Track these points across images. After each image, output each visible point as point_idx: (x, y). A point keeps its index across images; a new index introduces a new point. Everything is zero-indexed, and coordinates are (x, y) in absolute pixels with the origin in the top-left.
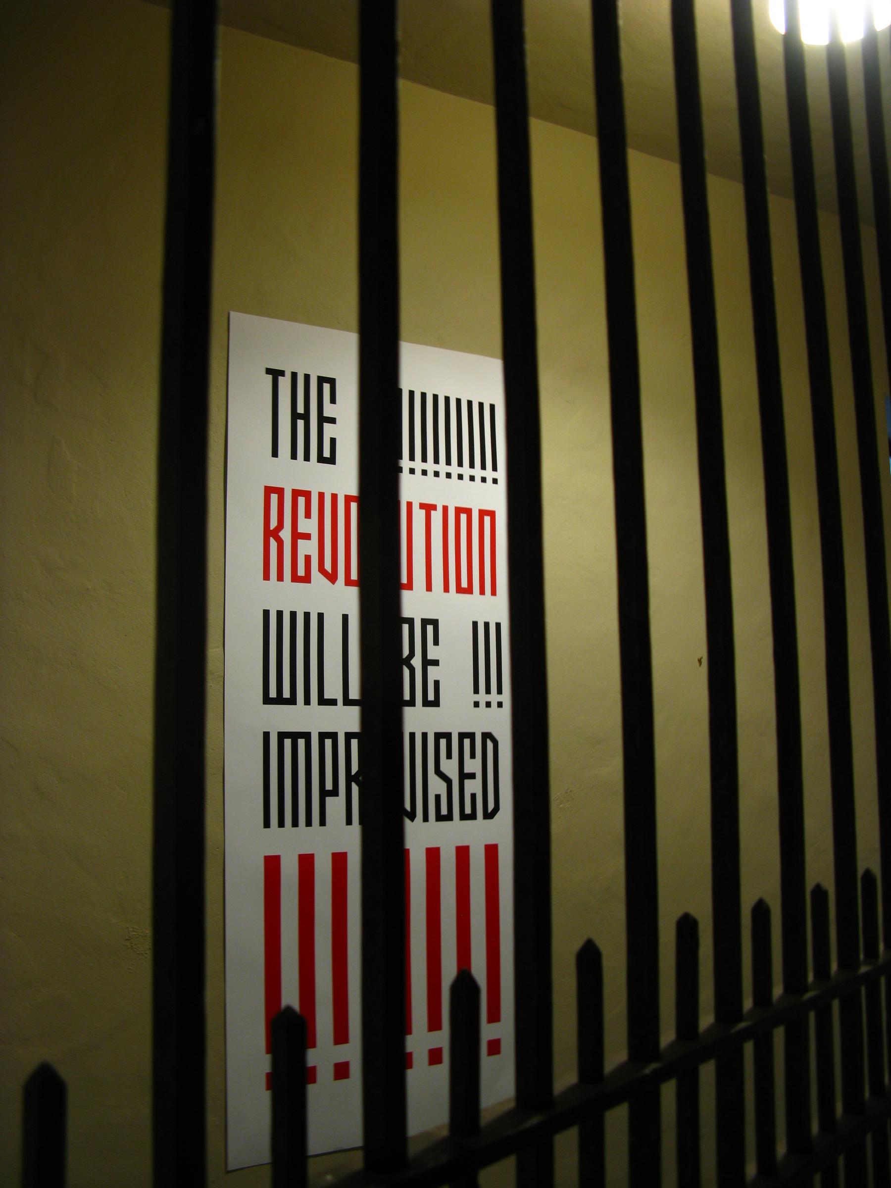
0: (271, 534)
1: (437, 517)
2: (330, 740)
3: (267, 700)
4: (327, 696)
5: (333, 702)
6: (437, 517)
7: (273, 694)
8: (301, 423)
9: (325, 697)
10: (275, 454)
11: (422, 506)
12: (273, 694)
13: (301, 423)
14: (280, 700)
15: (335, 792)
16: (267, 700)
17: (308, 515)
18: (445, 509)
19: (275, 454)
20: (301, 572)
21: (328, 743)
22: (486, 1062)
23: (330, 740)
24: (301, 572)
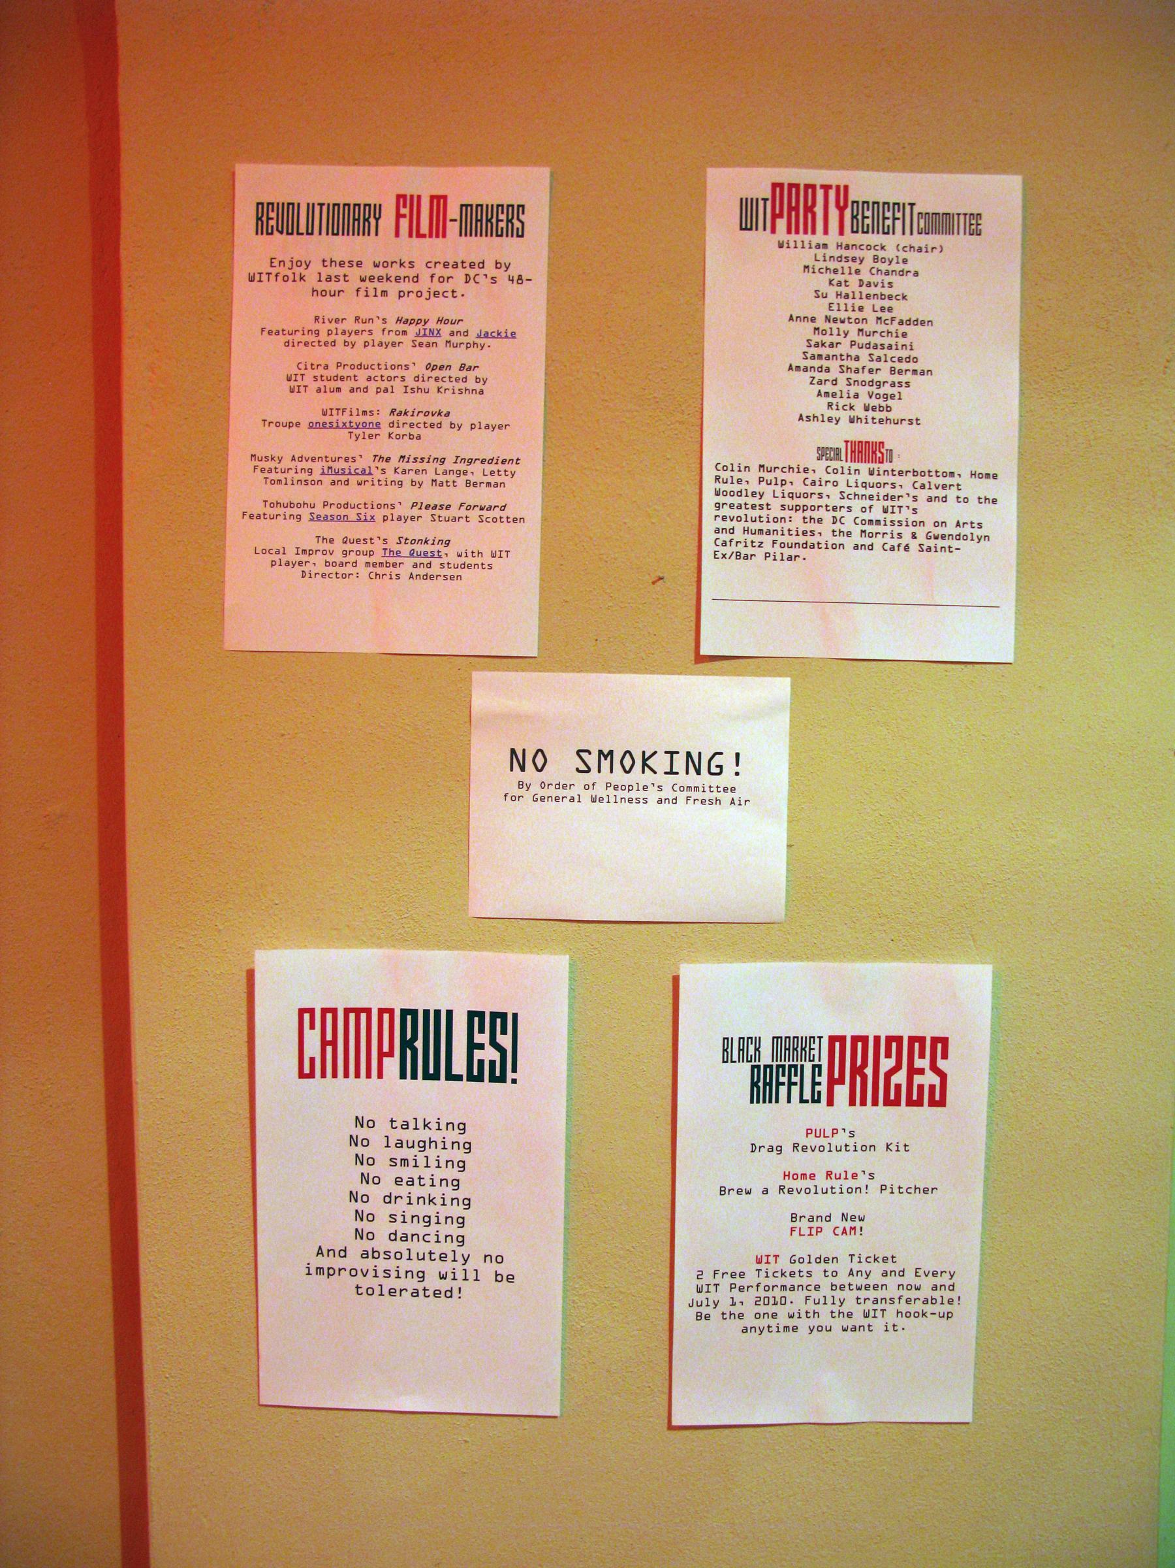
0: (259, 219)
1: (325, 208)
2: (388, 1015)
3: (741, 229)
4: (455, 1072)
5: (302, 234)
6: (325, 208)
7: (744, 227)
8: (329, 1049)
9: (915, 1067)
10: (397, 234)
11: (319, 204)
12: (744, 227)
13: (741, 1052)
14: (746, 229)
15: (391, 1054)
16: (741, 229)
17: (889, 211)
18: (329, 205)
19: (397, 234)
20: (270, 231)
21: (788, 1040)
22: (449, 224)
23: (388, 1015)
24: (270, 231)
